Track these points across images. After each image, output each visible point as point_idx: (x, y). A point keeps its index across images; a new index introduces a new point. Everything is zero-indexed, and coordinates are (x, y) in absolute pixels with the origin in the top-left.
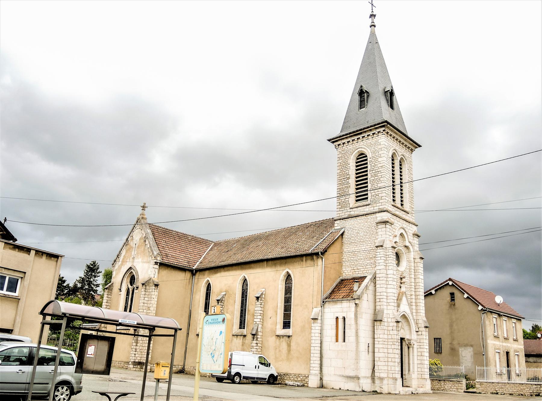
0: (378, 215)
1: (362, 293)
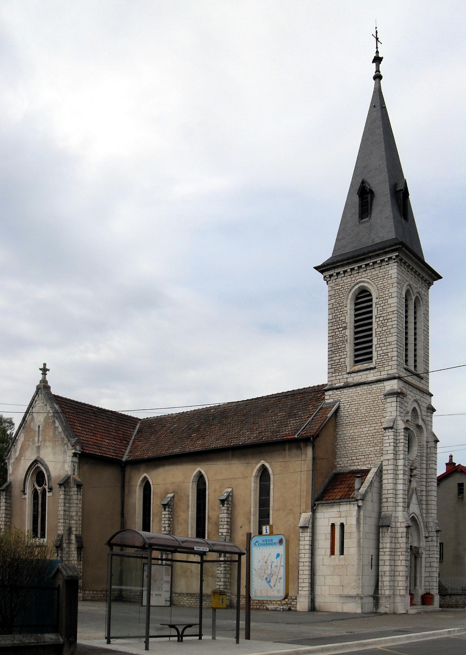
0: (386, 383)
1: (366, 492)
